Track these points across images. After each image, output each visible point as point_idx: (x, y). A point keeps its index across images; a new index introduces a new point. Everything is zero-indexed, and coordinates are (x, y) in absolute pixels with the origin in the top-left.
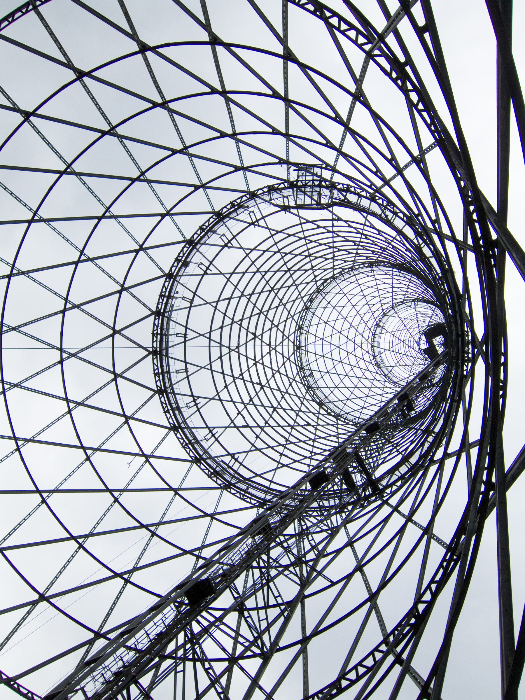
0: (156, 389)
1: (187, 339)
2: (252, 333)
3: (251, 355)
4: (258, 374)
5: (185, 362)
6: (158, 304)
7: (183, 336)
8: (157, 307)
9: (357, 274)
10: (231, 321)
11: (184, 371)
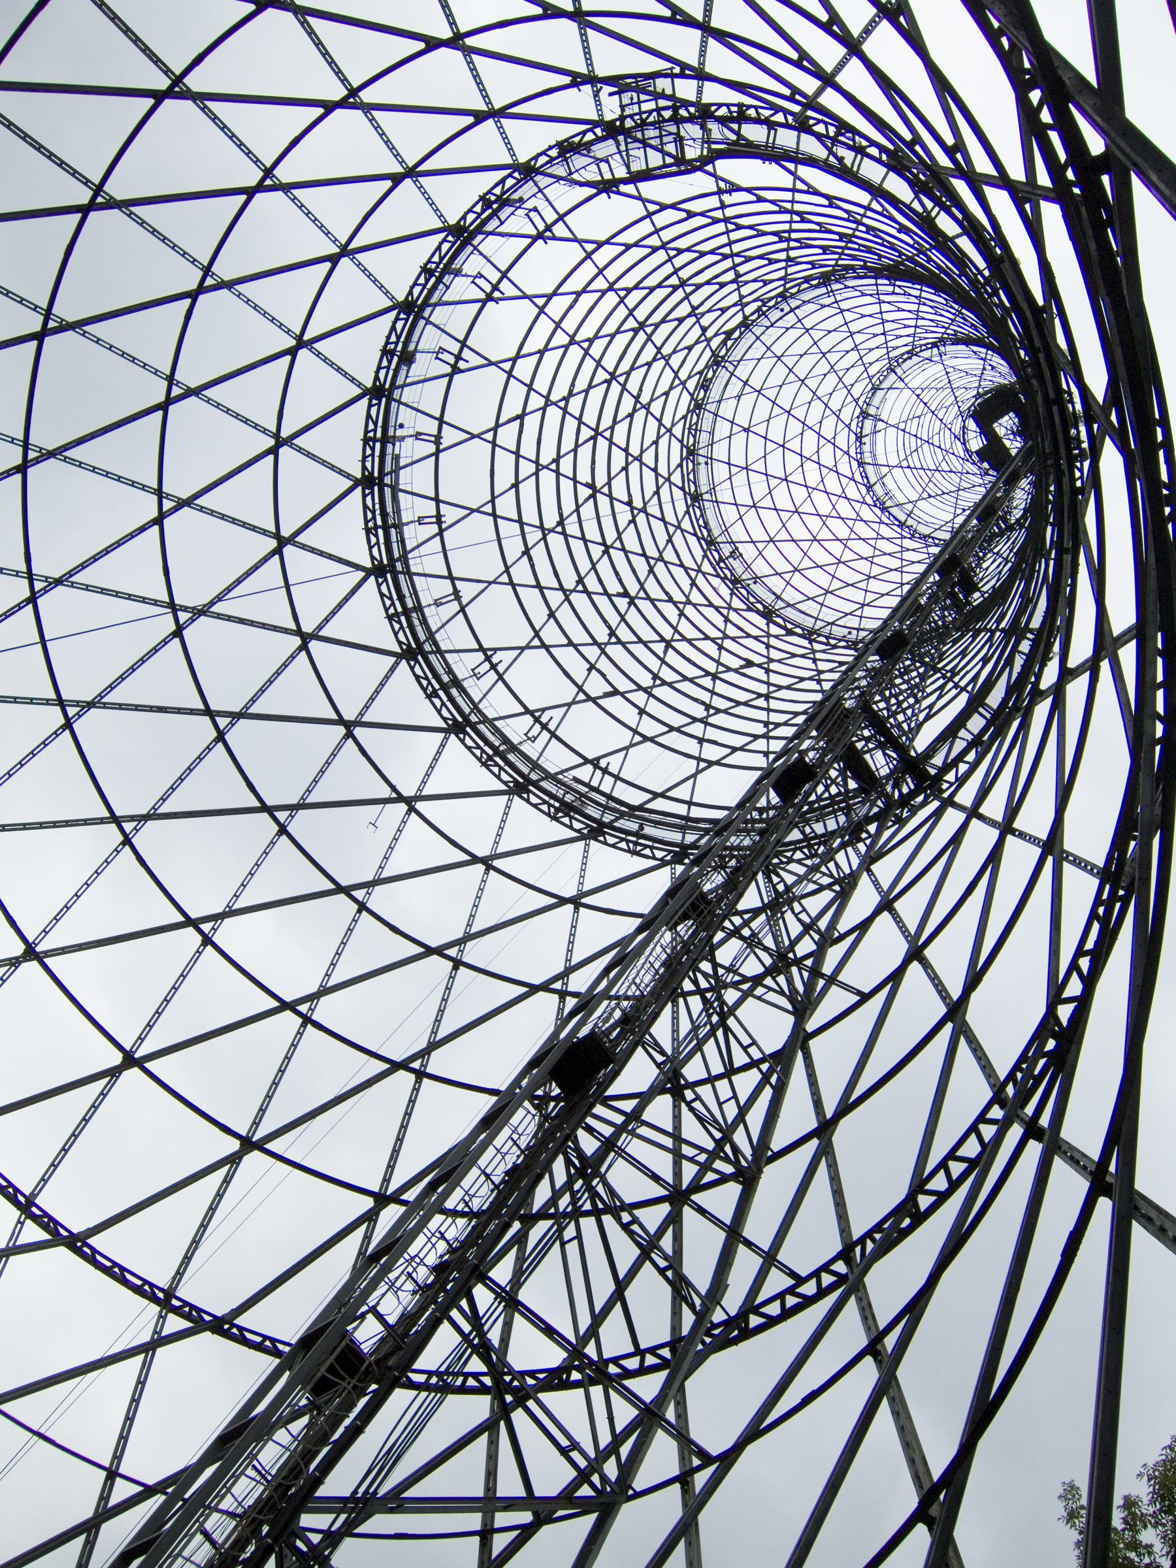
1: (444, 526)
2: (587, 485)
5: (451, 577)
7: (434, 520)
8: (364, 468)
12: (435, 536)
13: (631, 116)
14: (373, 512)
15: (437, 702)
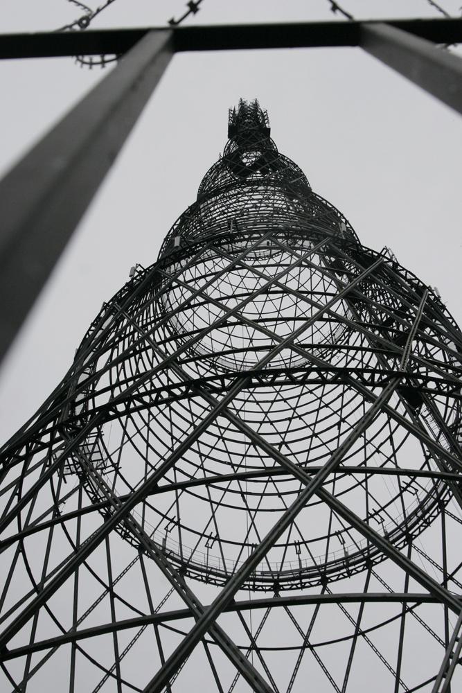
0: (367, 570)
3: (305, 445)
4: (328, 429)
5: (328, 537)
8: (269, 590)
9: (181, 324)
10: (269, 483)
11: (339, 536)
13: (76, 469)
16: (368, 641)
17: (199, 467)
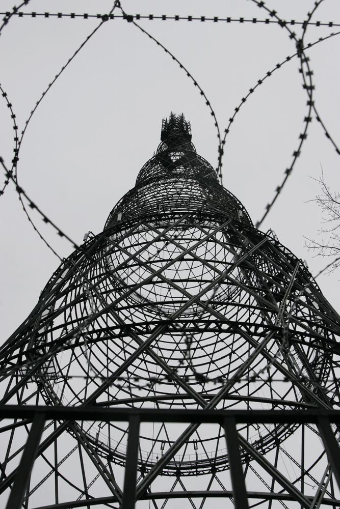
2: (186, 370)
4: (222, 358)
5: (218, 438)
6: (170, 475)
8: (173, 475)
12: (202, 444)
14: (190, 472)
15: (267, 450)
16: (311, 477)
17: (105, 367)
